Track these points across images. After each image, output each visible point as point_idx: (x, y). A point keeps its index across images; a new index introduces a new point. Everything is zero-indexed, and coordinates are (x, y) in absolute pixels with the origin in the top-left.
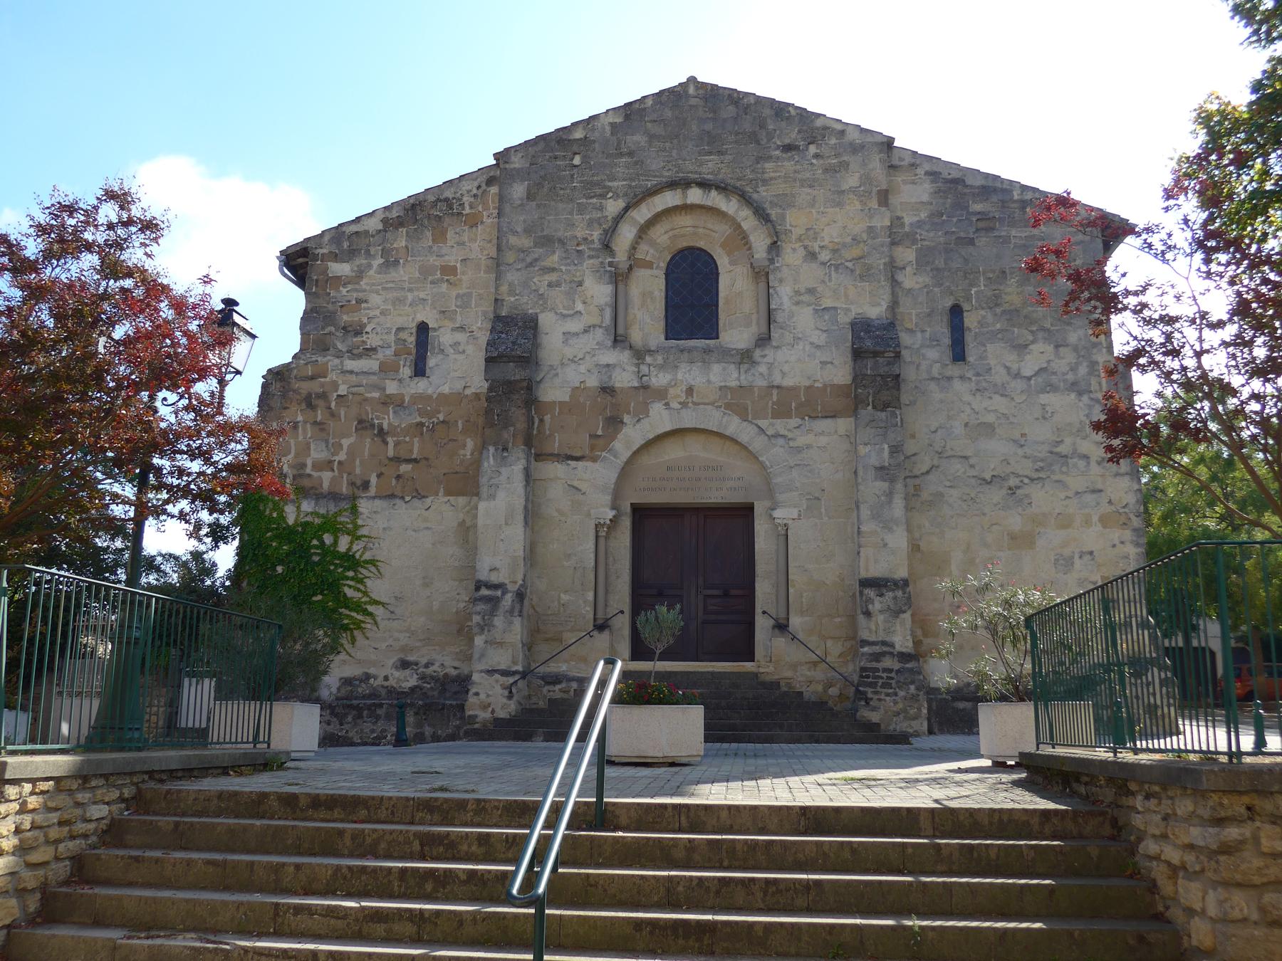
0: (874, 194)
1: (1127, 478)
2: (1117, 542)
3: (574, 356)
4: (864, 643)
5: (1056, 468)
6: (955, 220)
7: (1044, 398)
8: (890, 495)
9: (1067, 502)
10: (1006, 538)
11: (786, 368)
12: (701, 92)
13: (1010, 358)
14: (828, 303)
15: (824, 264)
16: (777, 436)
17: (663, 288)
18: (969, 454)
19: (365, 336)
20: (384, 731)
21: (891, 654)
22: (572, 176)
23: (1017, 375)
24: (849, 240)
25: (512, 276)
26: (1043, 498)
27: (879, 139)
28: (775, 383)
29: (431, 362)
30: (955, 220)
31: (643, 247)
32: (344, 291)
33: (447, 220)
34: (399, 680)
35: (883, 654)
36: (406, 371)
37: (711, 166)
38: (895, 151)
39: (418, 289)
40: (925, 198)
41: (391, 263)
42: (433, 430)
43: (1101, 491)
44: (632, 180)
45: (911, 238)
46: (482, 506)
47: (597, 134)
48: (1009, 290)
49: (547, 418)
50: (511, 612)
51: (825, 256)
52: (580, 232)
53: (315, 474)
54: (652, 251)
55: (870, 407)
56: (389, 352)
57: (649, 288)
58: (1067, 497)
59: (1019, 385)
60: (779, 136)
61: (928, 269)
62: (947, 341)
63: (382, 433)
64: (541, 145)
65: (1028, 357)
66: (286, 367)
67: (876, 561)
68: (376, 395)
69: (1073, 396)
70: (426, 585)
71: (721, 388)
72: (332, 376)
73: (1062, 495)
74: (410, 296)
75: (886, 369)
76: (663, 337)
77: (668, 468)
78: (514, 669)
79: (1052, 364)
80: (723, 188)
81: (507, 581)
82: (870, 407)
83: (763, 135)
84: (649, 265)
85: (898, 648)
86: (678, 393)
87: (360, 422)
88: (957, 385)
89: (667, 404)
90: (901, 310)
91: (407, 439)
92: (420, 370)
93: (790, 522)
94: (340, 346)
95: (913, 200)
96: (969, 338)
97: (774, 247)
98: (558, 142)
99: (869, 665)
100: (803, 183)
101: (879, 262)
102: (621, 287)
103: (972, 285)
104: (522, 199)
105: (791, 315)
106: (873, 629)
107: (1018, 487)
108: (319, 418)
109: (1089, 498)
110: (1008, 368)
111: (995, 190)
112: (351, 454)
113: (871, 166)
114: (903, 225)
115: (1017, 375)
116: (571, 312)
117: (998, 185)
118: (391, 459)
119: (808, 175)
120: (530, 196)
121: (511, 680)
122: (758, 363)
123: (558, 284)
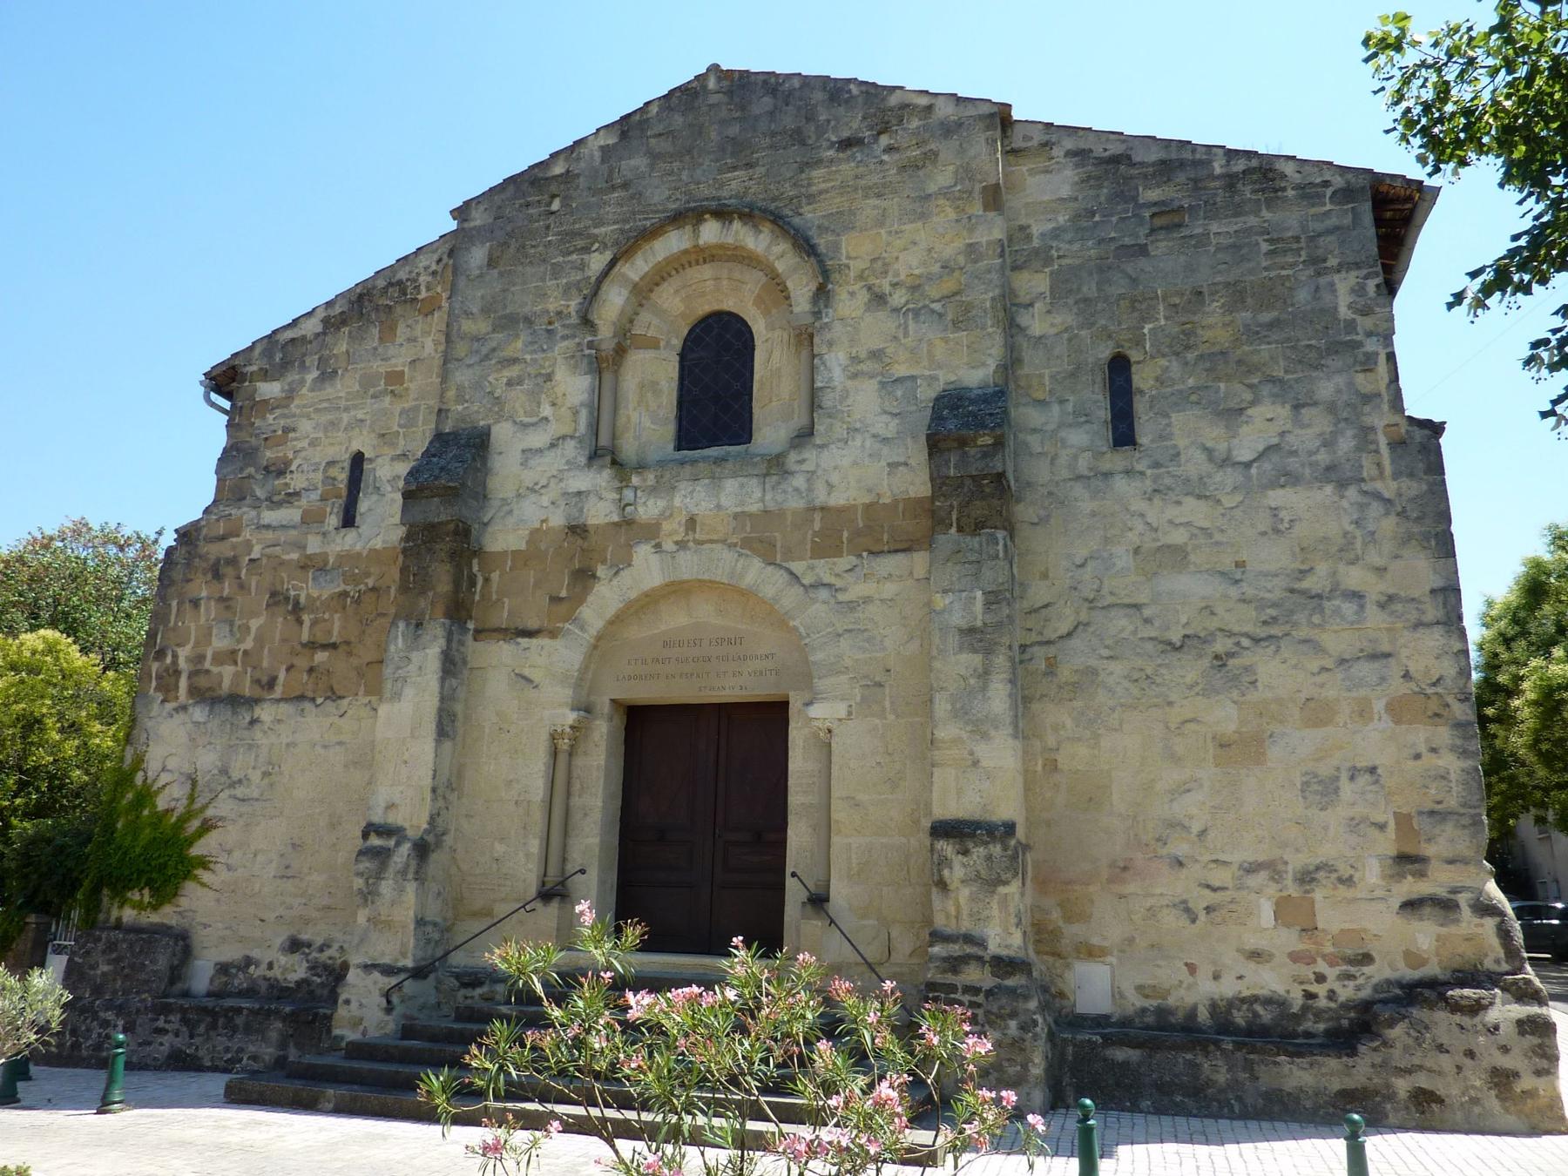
0: (976, 194)
1: (1438, 632)
2: (1423, 749)
3: (535, 486)
4: (937, 937)
5: (1300, 617)
6: (1114, 219)
7: (1276, 497)
8: (985, 674)
9: (1324, 676)
10: (1210, 745)
11: (835, 478)
12: (725, 83)
13: (1213, 434)
14: (901, 370)
15: (896, 310)
16: (818, 585)
17: (675, 375)
18: (1142, 598)
19: (288, 476)
20: (241, 1050)
21: (979, 959)
22: (548, 227)
23: (1226, 462)
24: (936, 268)
25: (462, 376)
26: (1277, 673)
27: (986, 109)
28: (818, 503)
29: (363, 505)
30: (1114, 219)
31: (645, 317)
32: (270, 418)
33: (399, 310)
34: (285, 970)
35: (965, 959)
36: (333, 521)
37: (735, 184)
38: (1018, 132)
39: (355, 407)
40: (1065, 191)
41: (328, 376)
42: (358, 602)
43: (1388, 655)
44: (625, 221)
45: (1042, 257)
46: (383, 710)
47: (582, 165)
48: (1211, 320)
49: (495, 576)
50: (403, 873)
51: (899, 298)
52: (552, 306)
53: (215, 670)
54: (655, 321)
55: (953, 530)
56: (315, 496)
57: (652, 382)
58: (1324, 669)
59: (1231, 477)
60: (835, 129)
61: (1071, 301)
62: (1104, 413)
63: (297, 609)
65: (1244, 429)
66: (195, 525)
67: (960, 792)
68: (295, 556)
69: (1329, 489)
70: (333, 826)
71: (736, 516)
72: (247, 534)
73: (1314, 665)
74: (345, 417)
75: (980, 465)
76: (671, 446)
77: (665, 644)
78: (400, 964)
79: (1290, 438)
80: (749, 214)
81: (406, 825)
82: (953, 530)
83: (810, 130)
84: (653, 344)
85: (994, 947)
86: (673, 528)
87: (273, 594)
88: (1120, 484)
89: (658, 546)
90: (1026, 370)
91: (327, 616)
92: (349, 521)
93: (834, 727)
94: (259, 493)
95: (1046, 198)
96: (1140, 406)
97: (822, 294)
98: (532, 183)
99: (939, 978)
100: (868, 192)
101: (984, 296)
102: (607, 376)
103: (1144, 320)
104: (480, 268)
105: (845, 394)
106: (958, 907)
107: (1231, 655)
108: (225, 593)
109: (1365, 669)
110: (1209, 452)
111: (1182, 164)
112: (260, 640)
113: (972, 152)
114: (1029, 238)
115: (1226, 462)
116: (535, 419)
117: (1187, 155)
118: (304, 646)
120: (492, 262)
121: (394, 981)
123: (520, 383)
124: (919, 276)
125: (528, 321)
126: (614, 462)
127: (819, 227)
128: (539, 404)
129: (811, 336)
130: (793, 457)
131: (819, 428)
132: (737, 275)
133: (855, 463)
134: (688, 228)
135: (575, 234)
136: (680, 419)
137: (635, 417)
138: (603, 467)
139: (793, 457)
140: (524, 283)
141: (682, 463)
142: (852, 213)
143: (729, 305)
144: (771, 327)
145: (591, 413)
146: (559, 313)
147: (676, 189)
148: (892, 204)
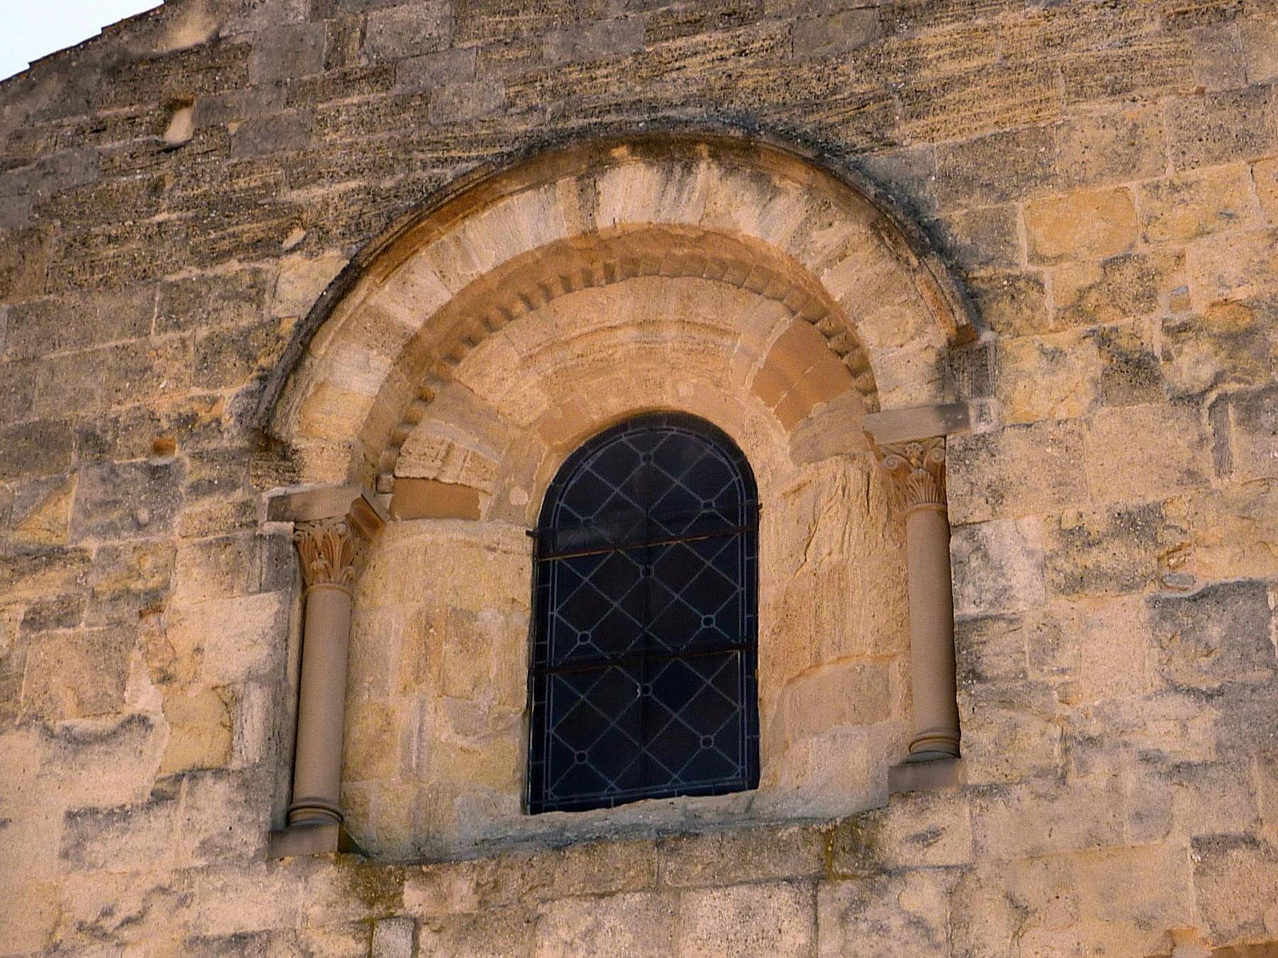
14: (1218, 566)
15: (1189, 399)
17: (523, 591)
22: (156, 188)
31: (436, 428)
37: (697, 66)
51: (1193, 365)
54: (466, 442)
57: (452, 633)
64: (53, 86)
76: (512, 800)
80: (744, 145)
84: (460, 504)
97: (966, 358)
98: (113, 72)
100: (1081, 82)
102: (325, 597)
105: (1051, 639)
116: (107, 723)
119: (1102, 46)
122: (900, 873)
123: (66, 614)
124: (1250, 306)
125: (94, 444)
126: (347, 847)
127: (946, 176)
128: (122, 680)
129: (938, 475)
130: (899, 825)
131: (978, 736)
132: (705, 313)
133: (1093, 841)
134: (566, 185)
135: (231, 205)
136: (537, 719)
137: (405, 713)
138: (313, 860)
139: (899, 825)
140: (87, 338)
141: (559, 846)
142: (1041, 137)
143: (681, 393)
144: (809, 453)
145: (277, 701)
146: (187, 422)
147: (528, 82)
148: (1156, 112)
